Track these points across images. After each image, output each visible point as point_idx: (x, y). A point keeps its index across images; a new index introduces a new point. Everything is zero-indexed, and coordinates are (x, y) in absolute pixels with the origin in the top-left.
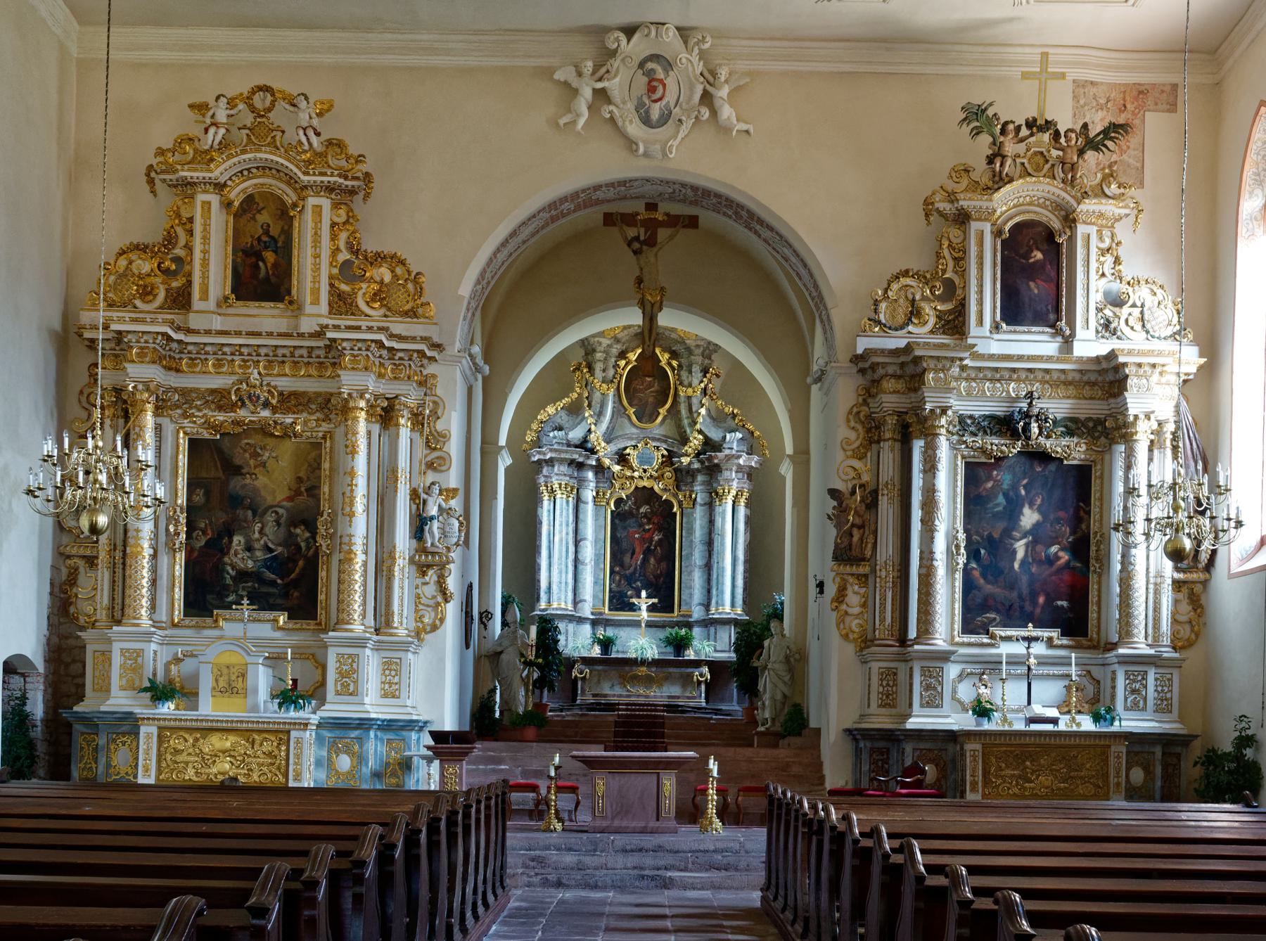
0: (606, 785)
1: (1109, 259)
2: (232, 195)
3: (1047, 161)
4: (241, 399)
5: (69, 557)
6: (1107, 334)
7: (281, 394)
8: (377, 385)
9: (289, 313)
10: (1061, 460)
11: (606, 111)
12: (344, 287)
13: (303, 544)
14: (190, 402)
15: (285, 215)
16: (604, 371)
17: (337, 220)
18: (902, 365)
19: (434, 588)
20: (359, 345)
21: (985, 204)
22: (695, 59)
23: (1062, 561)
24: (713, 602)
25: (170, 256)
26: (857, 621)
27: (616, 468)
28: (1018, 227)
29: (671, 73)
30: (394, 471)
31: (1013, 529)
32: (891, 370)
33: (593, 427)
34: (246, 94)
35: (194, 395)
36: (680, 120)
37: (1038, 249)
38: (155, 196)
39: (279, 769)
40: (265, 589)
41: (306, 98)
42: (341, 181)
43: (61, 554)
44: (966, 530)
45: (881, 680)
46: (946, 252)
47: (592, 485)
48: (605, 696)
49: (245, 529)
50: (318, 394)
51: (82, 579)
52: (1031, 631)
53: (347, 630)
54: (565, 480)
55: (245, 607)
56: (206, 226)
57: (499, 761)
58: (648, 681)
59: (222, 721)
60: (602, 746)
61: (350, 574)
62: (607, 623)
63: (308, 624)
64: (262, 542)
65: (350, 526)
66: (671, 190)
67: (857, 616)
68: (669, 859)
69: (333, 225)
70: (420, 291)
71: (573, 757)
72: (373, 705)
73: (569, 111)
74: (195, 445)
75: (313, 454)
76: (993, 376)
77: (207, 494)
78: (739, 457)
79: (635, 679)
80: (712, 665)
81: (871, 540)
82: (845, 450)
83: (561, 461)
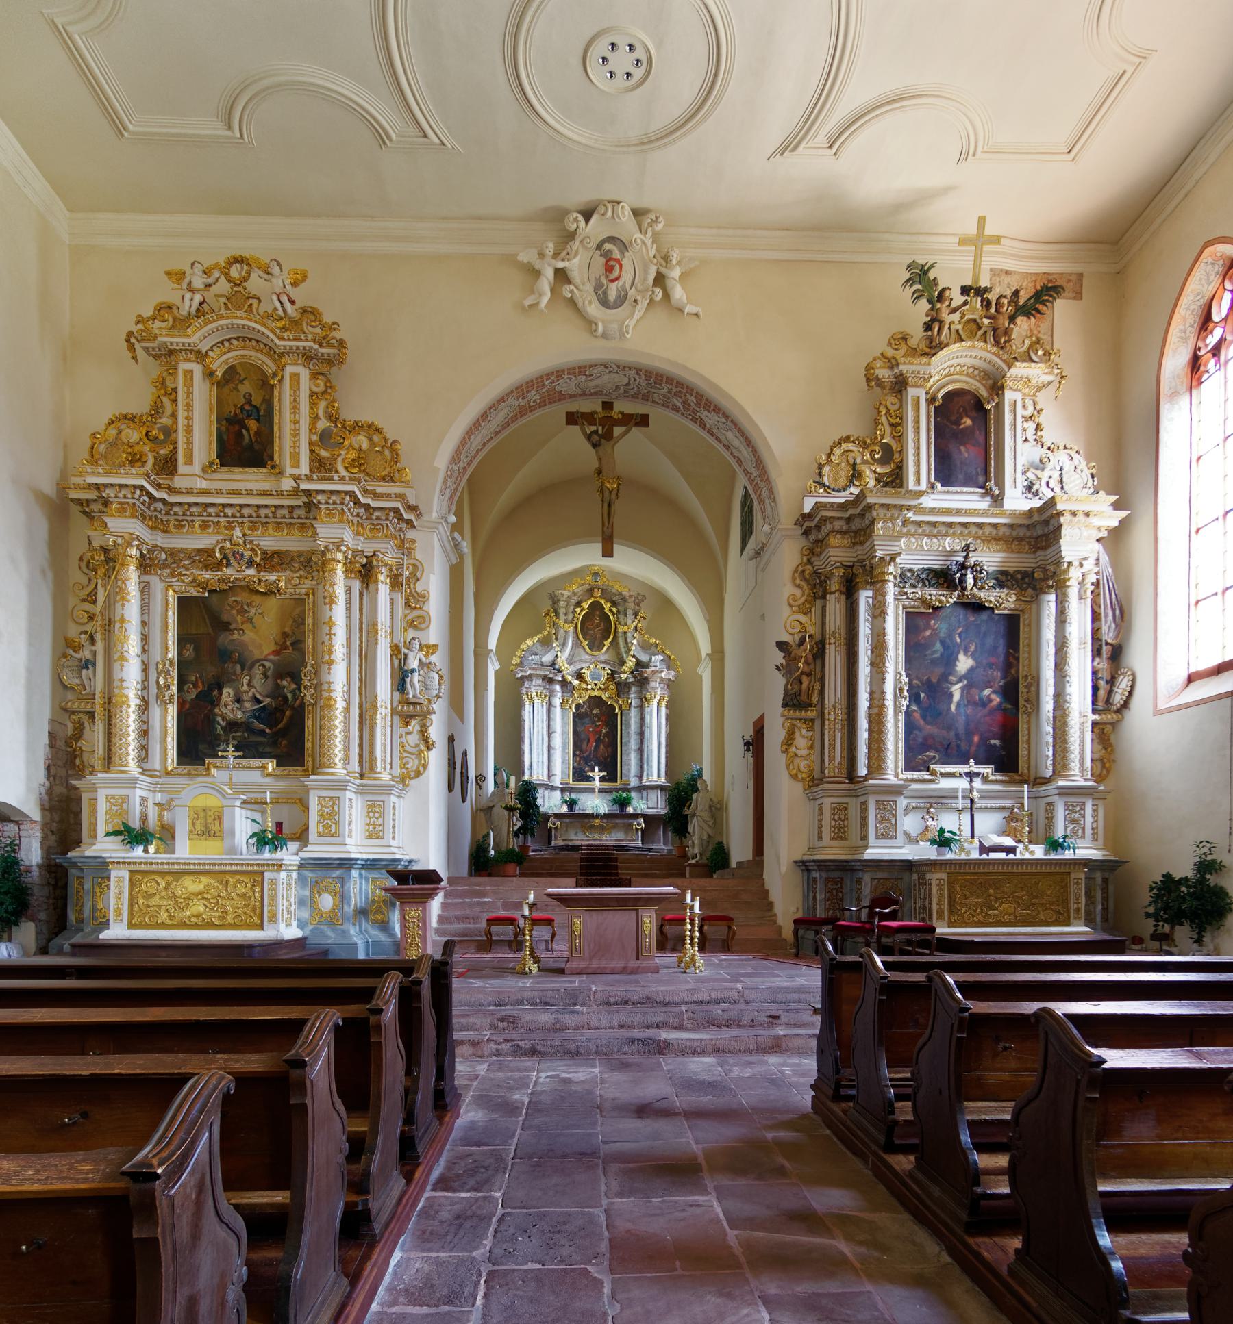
0: (584, 923)
1: (1031, 426)
2: (214, 367)
3: (979, 328)
4: (225, 557)
5: (73, 713)
6: (1030, 496)
7: (264, 552)
8: (356, 542)
9: (273, 479)
10: (992, 609)
11: (567, 291)
12: (324, 453)
13: (289, 696)
14: (178, 562)
15: (266, 385)
16: (566, 614)
17: (315, 389)
18: (849, 520)
19: (417, 737)
20: (334, 498)
21: (922, 369)
22: (649, 241)
23: (995, 703)
24: (645, 774)
25: (158, 425)
26: (806, 762)
27: (576, 682)
28: (949, 395)
29: (626, 254)
30: (375, 625)
31: (950, 674)
32: (838, 525)
33: (559, 654)
34: (223, 264)
35: (182, 555)
36: (635, 301)
37: (968, 416)
38: (137, 362)
39: (254, 910)
40: (253, 738)
41: (279, 264)
42: (316, 347)
43: (65, 710)
44: (907, 675)
45: (834, 814)
46: (883, 419)
47: (559, 694)
48: (572, 840)
49: (232, 680)
50: (300, 554)
51: (87, 732)
52: (972, 767)
53: (328, 774)
54: (540, 690)
55: (230, 754)
56: (189, 394)
57: (484, 895)
58: (601, 829)
59: (226, 864)
60: (573, 881)
61: (330, 719)
62: (572, 790)
63: (296, 770)
64: (250, 694)
65: (329, 673)
66: (625, 381)
67: (804, 757)
68: (659, 1015)
69: (312, 394)
70: (396, 456)
71: (549, 895)
72: (356, 845)
73: (532, 292)
74: (185, 603)
75: (298, 611)
76: (931, 531)
77: (196, 649)
78: (662, 671)
79: (592, 827)
80: (645, 817)
81: (817, 687)
82: (791, 606)
83: (538, 676)
